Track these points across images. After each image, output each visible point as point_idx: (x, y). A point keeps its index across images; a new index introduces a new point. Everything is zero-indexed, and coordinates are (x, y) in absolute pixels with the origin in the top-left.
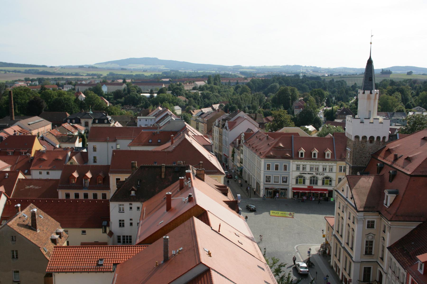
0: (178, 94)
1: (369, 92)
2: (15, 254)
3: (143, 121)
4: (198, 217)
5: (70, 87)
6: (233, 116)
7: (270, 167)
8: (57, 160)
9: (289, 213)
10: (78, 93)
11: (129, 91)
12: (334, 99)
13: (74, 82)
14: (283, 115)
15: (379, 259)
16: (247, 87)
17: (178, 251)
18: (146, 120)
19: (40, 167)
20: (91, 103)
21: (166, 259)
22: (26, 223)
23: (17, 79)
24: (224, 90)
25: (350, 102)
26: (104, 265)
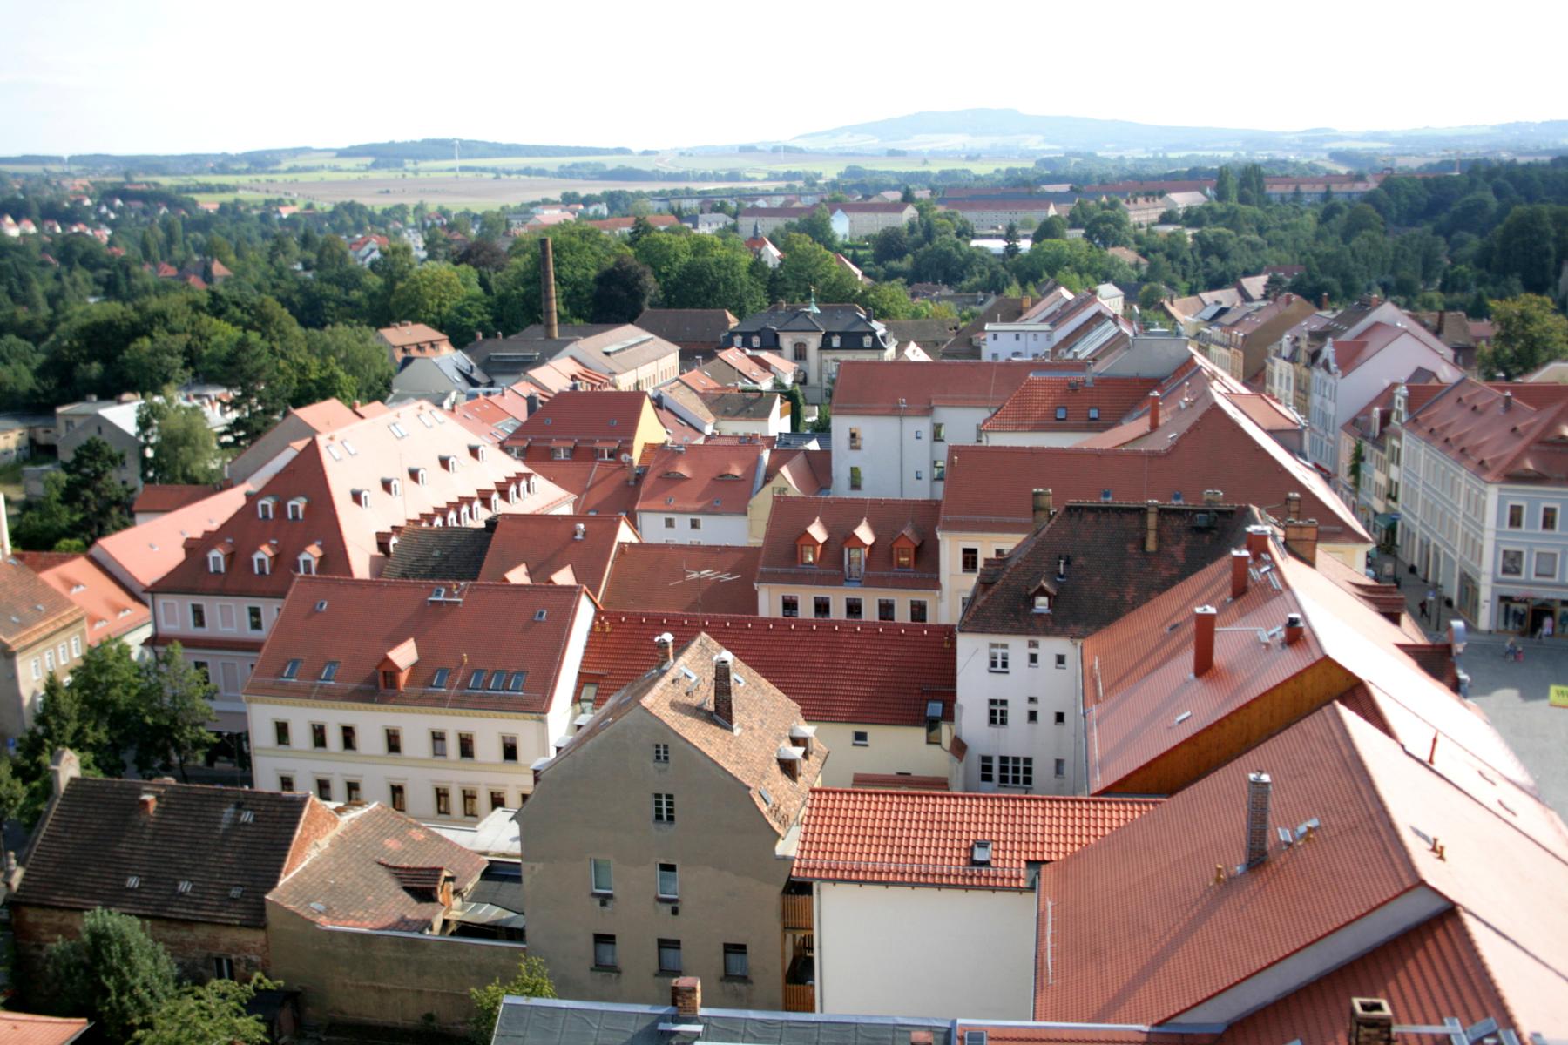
0: (1109, 239)
2: (664, 807)
3: (1001, 342)
4: (1343, 702)
5: (720, 220)
6: (1350, 319)
8: (723, 478)
10: (755, 241)
11: (929, 233)
13: (732, 205)
16: (1370, 210)
18: (1017, 337)
19: (667, 504)
20: (805, 275)
21: (1258, 860)
22: (695, 700)
23: (537, 197)
24: (1279, 223)
26: (993, 863)
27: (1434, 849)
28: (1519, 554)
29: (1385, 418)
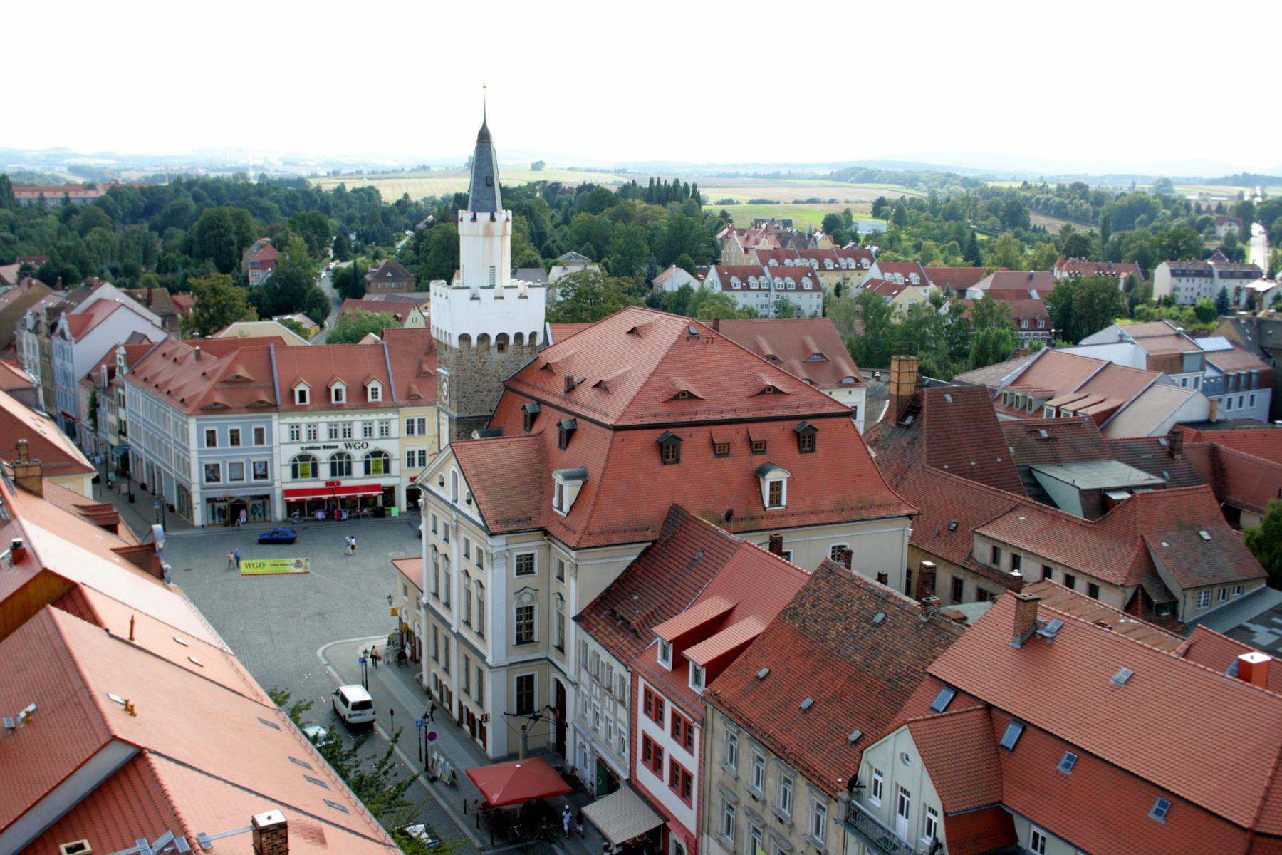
1: (487, 216)
4: (53, 605)
7: (214, 437)
9: (293, 560)
12: (353, 237)
14: (223, 287)
15: (553, 650)
16: (101, 212)
17: (23, 714)
25: (399, 245)
27: (126, 709)
28: (217, 466)
29: (111, 373)
